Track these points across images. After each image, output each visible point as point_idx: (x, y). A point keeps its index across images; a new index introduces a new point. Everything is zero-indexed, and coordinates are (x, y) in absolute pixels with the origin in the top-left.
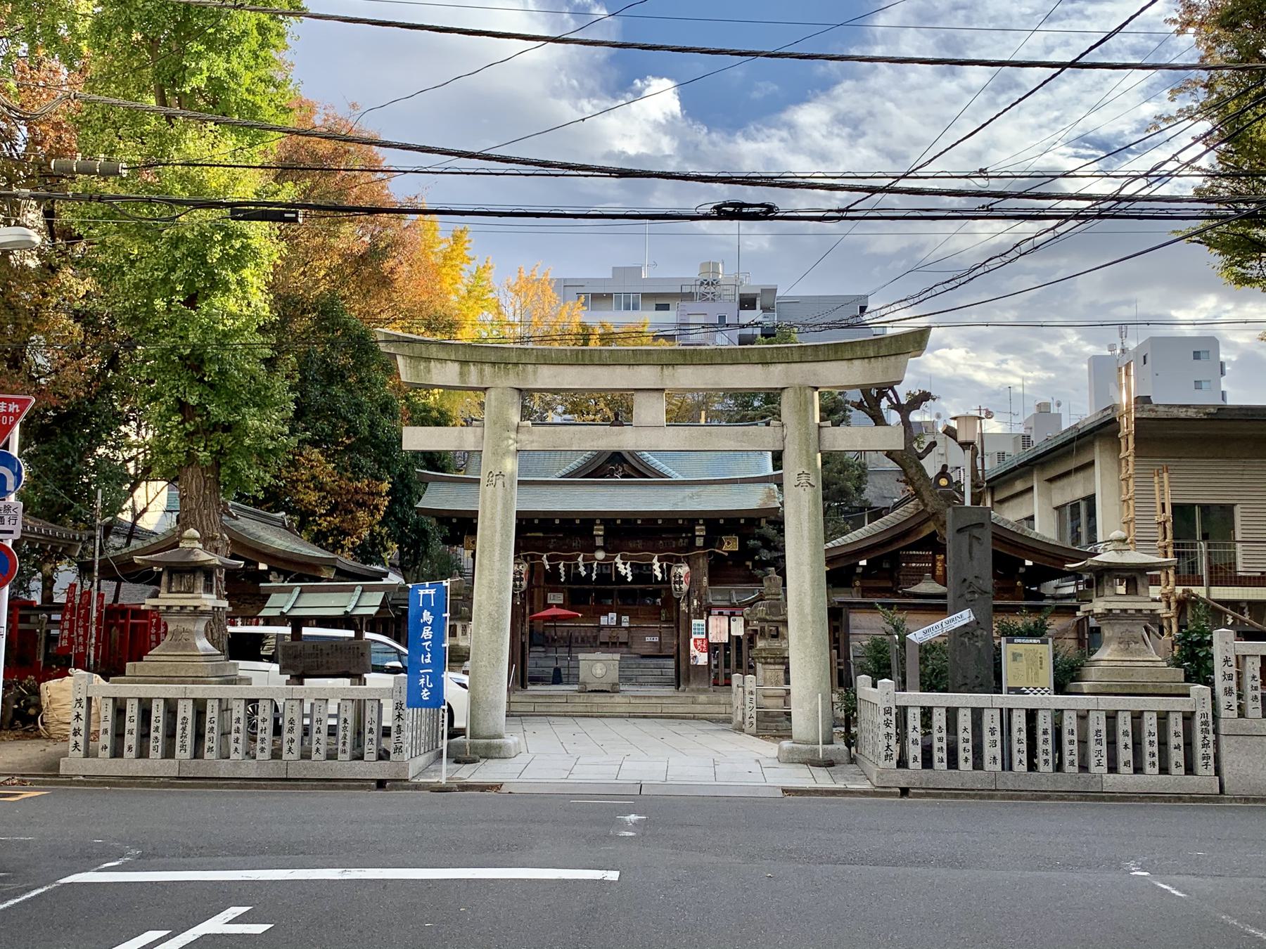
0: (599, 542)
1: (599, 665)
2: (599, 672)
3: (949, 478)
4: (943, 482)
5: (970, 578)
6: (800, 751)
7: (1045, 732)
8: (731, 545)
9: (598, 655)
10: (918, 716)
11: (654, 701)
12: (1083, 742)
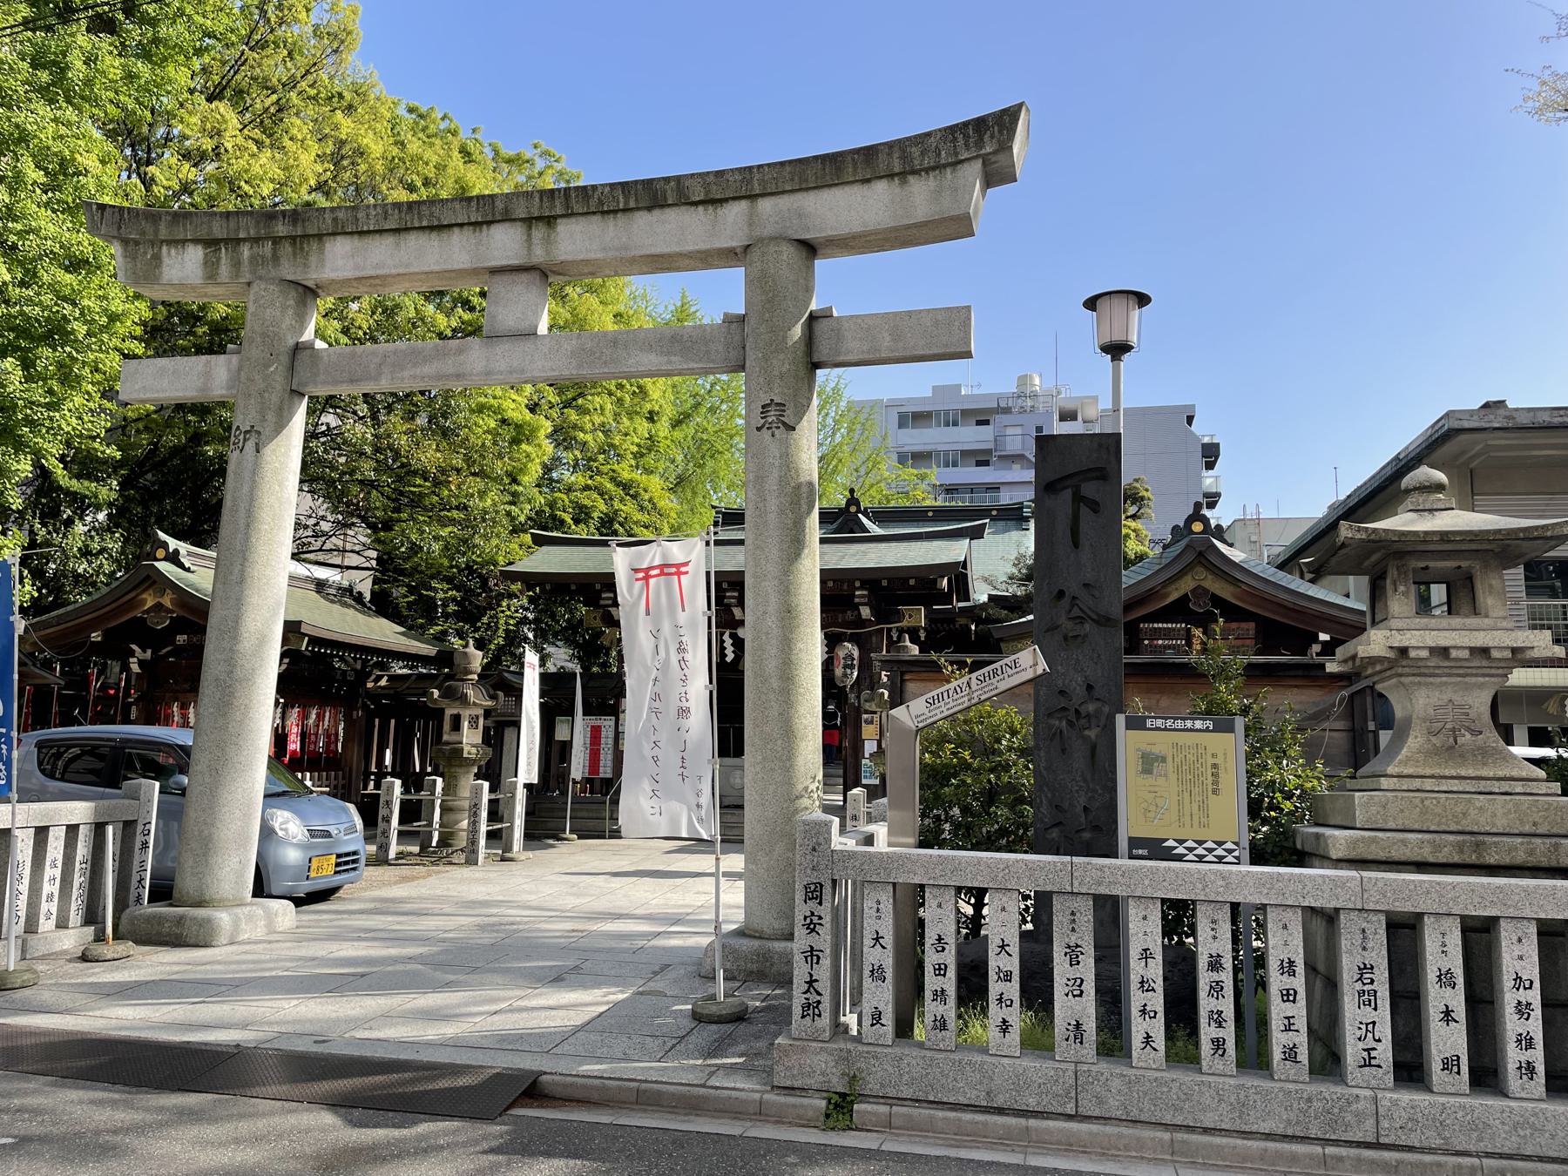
5: (1073, 588)
7: (1215, 965)
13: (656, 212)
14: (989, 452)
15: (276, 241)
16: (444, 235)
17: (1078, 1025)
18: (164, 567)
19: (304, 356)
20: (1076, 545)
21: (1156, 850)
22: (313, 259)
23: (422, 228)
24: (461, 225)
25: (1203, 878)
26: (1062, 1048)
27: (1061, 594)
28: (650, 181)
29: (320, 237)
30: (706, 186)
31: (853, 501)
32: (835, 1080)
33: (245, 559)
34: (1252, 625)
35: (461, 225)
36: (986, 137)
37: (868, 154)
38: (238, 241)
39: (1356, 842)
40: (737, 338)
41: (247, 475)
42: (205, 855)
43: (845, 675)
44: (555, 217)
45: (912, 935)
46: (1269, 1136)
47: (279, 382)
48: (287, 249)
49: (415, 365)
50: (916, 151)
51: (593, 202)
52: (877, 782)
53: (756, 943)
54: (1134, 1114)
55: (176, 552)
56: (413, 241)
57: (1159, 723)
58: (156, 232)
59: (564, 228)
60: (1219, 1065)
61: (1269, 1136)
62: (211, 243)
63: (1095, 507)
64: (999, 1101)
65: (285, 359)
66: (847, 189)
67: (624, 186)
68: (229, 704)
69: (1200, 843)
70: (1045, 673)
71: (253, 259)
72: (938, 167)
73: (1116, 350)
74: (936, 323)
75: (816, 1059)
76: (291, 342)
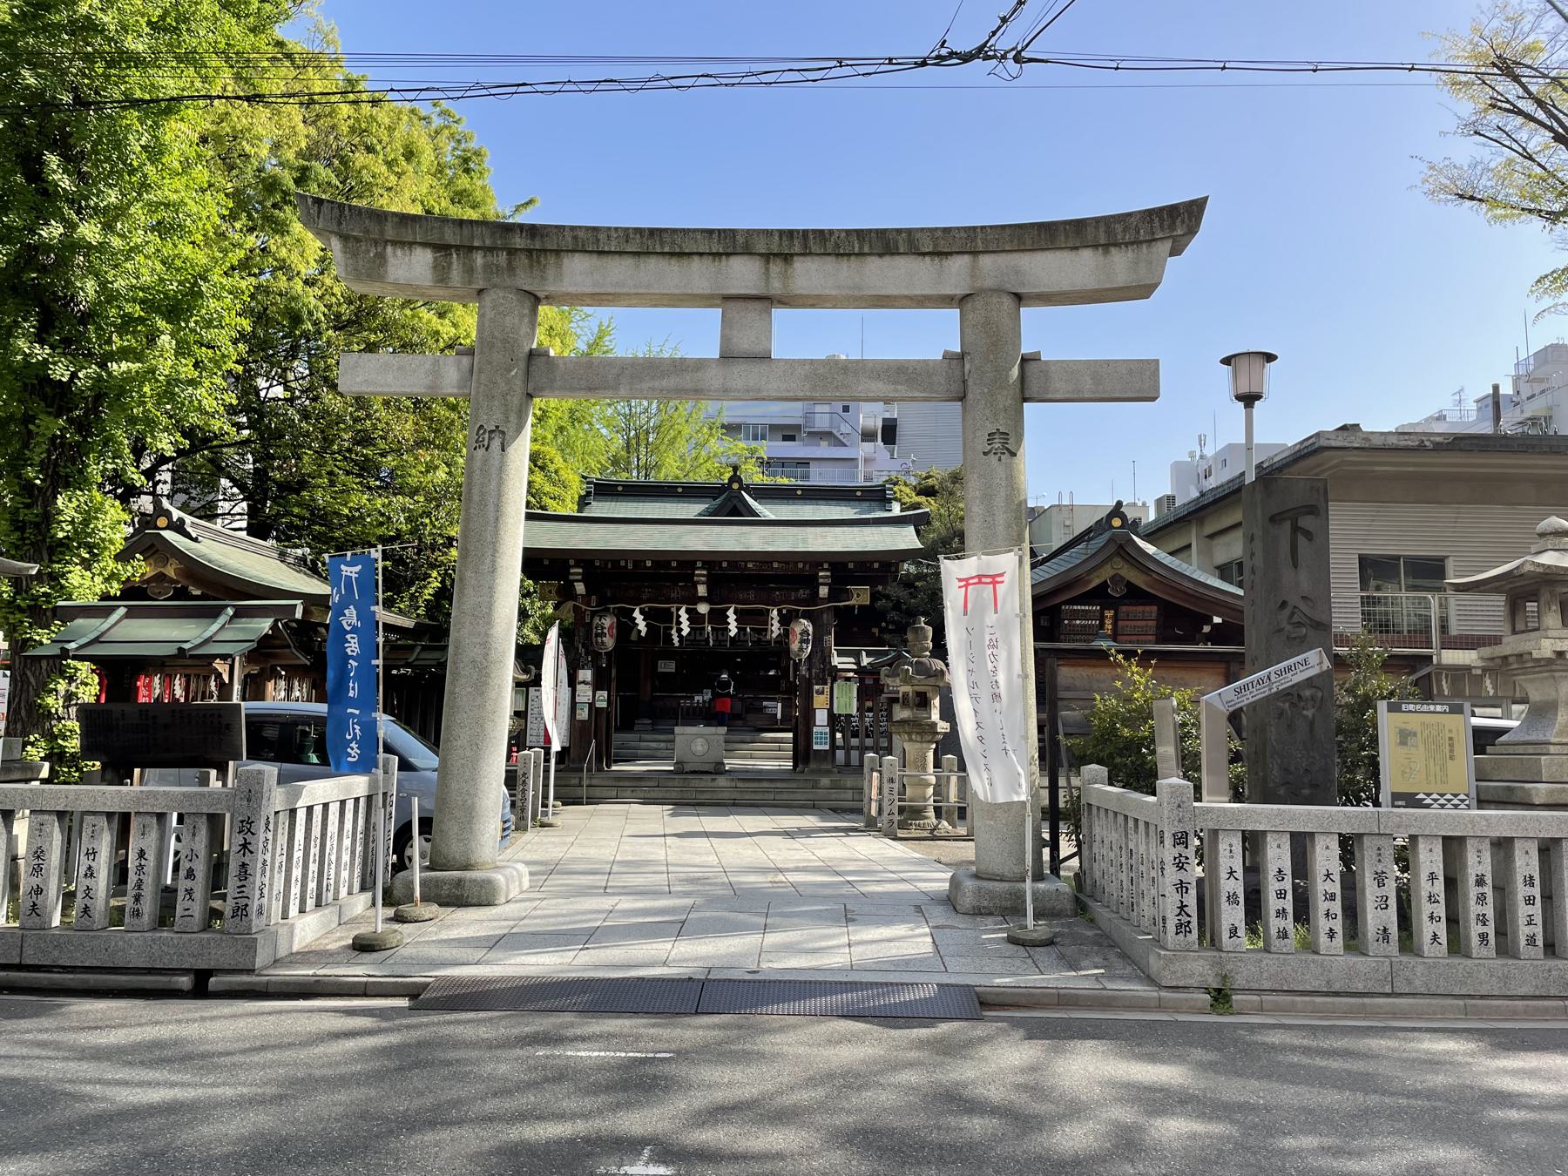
0: (702, 590)
1: (700, 741)
2: (699, 748)
3: (1123, 517)
4: (1117, 522)
5: (1294, 600)
6: (992, 895)
7: (1480, 882)
8: (860, 596)
9: (701, 729)
10: (1238, 848)
11: (765, 784)
12: (1503, 890)
13: (887, 259)
14: (798, 427)
15: (512, 252)
16: (685, 261)
17: (1385, 930)
18: (169, 535)
19: (539, 361)
20: (1295, 566)
21: (1411, 800)
22: (551, 272)
23: (663, 254)
24: (701, 254)
25: (1472, 821)
26: (1374, 947)
27: (1284, 604)
28: (885, 231)
29: (557, 252)
30: (935, 240)
31: (735, 478)
32: (1210, 979)
33: (496, 551)
34: (1155, 608)
35: (701, 254)
36: (1178, 222)
37: (1079, 226)
38: (471, 249)
39: (1552, 792)
40: (957, 373)
41: (494, 471)
42: (470, 822)
43: (801, 649)
44: (792, 255)
45: (1253, 869)
46: (1523, 997)
47: (518, 384)
48: (522, 260)
49: (653, 378)
50: (1119, 228)
51: (830, 247)
52: (827, 747)
53: (1006, 885)
54: (1433, 989)
55: (181, 521)
56: (653, 263)
57: (1411, 707)
58: (382, 232)
59: (801, 266)
60: (1484, 952)
61: (1523, 997)
62: (441, 248)
63: (1308, 535)
64: (1336, 987)
65: (522, 364)
66: (1058, 253)
67: (859, 233)
68: (486, 684)
69: (1442, 795)
70: (1328, 671)
71: (486, 267)
72: (1137, 243)
73: (1249, 399)
74: (1130, 372)
75: (1195, 964)
76: (527, 349)
